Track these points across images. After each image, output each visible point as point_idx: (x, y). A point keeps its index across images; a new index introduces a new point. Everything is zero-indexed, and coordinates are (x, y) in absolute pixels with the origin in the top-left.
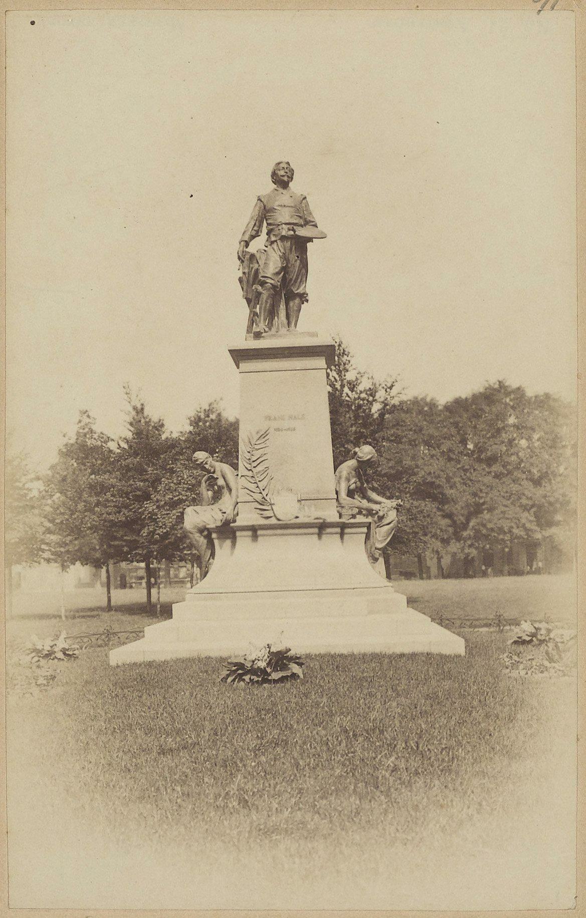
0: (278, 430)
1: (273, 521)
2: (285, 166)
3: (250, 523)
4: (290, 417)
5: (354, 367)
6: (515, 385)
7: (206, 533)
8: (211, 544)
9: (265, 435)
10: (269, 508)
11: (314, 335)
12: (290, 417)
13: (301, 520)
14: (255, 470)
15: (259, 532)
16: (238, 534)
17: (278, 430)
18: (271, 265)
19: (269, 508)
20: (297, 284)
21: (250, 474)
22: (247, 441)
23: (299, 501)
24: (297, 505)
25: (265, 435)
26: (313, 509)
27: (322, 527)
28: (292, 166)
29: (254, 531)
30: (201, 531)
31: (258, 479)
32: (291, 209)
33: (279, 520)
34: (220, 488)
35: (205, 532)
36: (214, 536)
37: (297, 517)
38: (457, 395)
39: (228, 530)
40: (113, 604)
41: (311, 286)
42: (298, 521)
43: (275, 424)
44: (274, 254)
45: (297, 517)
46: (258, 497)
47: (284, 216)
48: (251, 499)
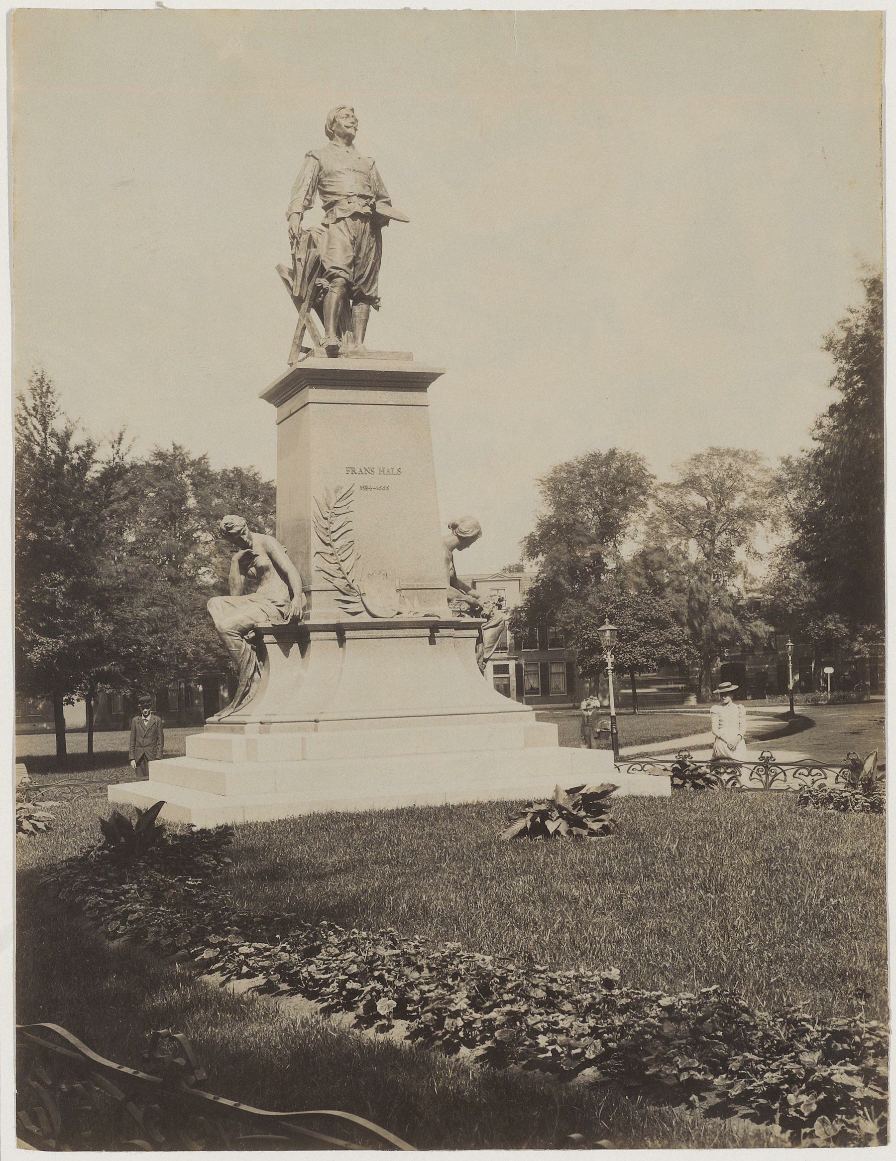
0: (365, 488)
1: (365, 618)
2: (351, 113)
3: (333, 621)
4: (382, 471)
5: (62, 410)
6: (194, 456)
7: (252, 635)
8: (262, 655)
9: (347, 495)
10: (358, 599)
11: (409, 357)
12: (382, 471)
13: (405, 617)
14: (337, 545)
15: (348, 634)
16: (313, 636)
17: (365, 488)
18: (337, 253)
19: (358, 599)
20: (369, 284)
21: (329, 550)
22: (322, 502)
23: (399, 590)
24: (396, 597)
25: (347, 495)
26: (416, 603)
27: (434, 627)
28: (357, 114)
29: (340, 631)
30: (243, 632)
31: (340, 558)
32: (358, 175)
33: (374, 616)
34: (262, 571)
35: (256, 637)
36: (267, 638)
37: (399, 613)
38: (243, 464)
39: (295, 634)
40: (94, 750)
41: (383, 287)
42: (397, 619)
43: (366, 479)
44: (339, 235)
45: (399, 613)
46: (341, 583)
47: (347, 184)
48: (330, 586)
